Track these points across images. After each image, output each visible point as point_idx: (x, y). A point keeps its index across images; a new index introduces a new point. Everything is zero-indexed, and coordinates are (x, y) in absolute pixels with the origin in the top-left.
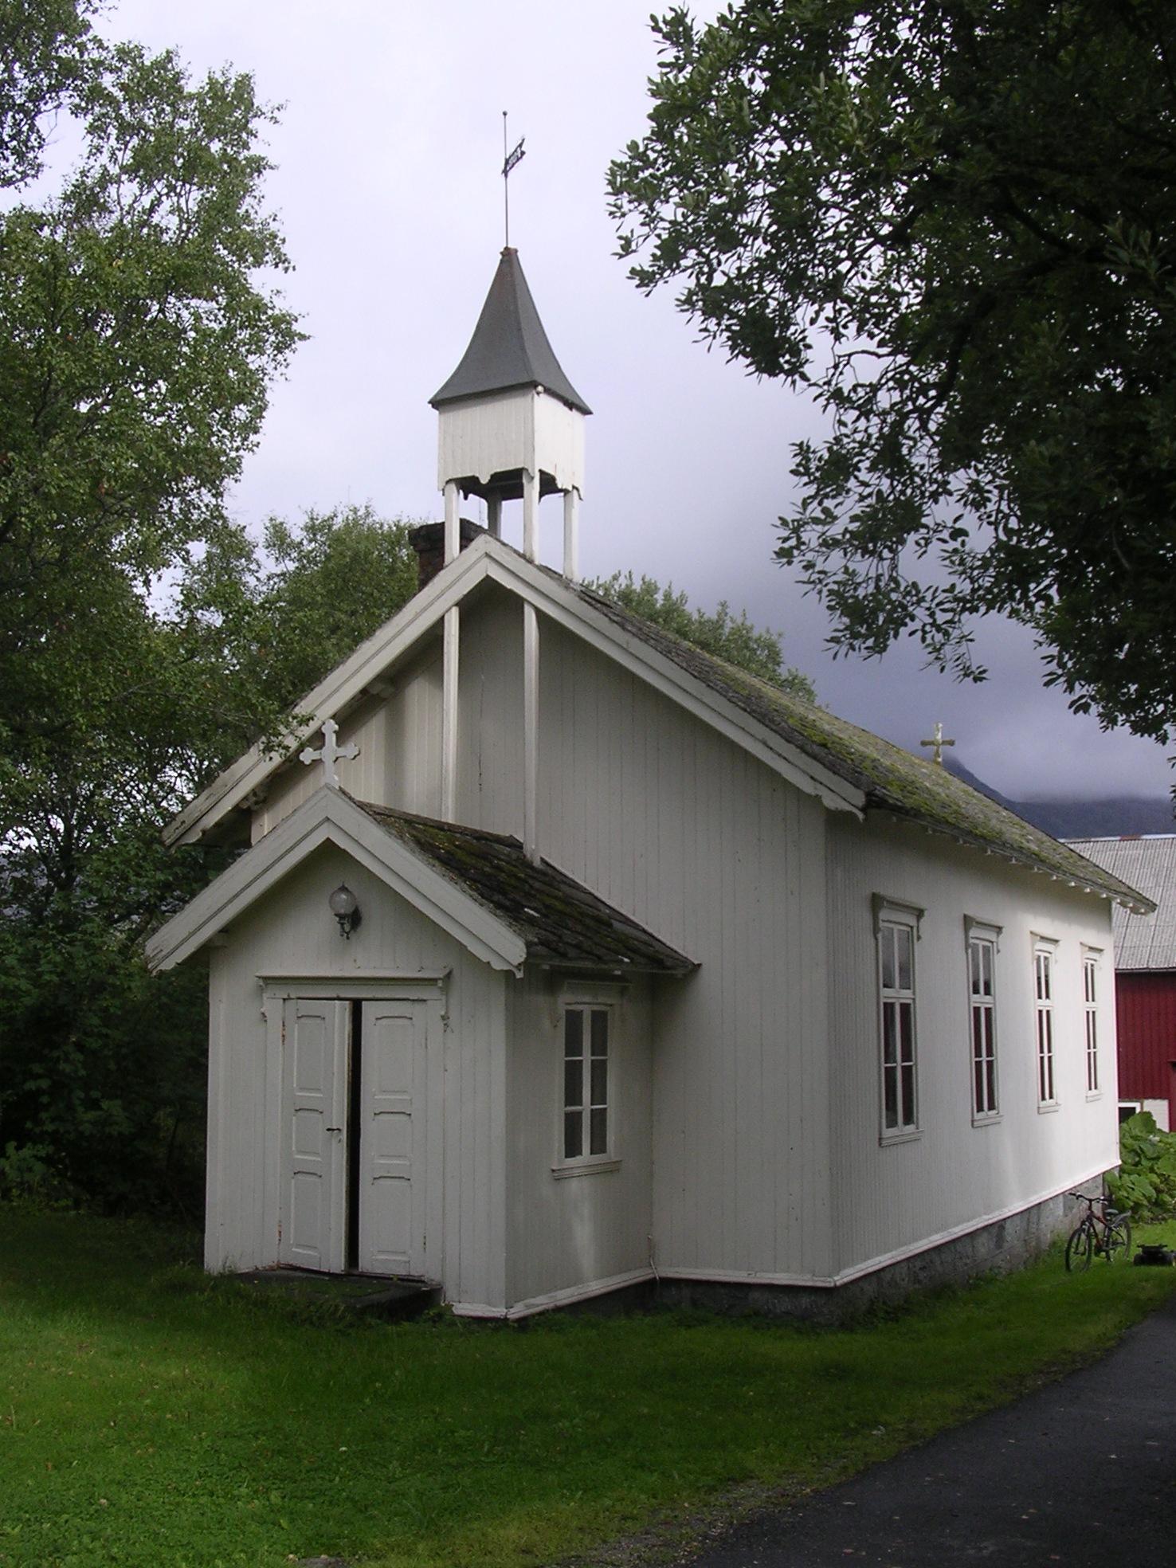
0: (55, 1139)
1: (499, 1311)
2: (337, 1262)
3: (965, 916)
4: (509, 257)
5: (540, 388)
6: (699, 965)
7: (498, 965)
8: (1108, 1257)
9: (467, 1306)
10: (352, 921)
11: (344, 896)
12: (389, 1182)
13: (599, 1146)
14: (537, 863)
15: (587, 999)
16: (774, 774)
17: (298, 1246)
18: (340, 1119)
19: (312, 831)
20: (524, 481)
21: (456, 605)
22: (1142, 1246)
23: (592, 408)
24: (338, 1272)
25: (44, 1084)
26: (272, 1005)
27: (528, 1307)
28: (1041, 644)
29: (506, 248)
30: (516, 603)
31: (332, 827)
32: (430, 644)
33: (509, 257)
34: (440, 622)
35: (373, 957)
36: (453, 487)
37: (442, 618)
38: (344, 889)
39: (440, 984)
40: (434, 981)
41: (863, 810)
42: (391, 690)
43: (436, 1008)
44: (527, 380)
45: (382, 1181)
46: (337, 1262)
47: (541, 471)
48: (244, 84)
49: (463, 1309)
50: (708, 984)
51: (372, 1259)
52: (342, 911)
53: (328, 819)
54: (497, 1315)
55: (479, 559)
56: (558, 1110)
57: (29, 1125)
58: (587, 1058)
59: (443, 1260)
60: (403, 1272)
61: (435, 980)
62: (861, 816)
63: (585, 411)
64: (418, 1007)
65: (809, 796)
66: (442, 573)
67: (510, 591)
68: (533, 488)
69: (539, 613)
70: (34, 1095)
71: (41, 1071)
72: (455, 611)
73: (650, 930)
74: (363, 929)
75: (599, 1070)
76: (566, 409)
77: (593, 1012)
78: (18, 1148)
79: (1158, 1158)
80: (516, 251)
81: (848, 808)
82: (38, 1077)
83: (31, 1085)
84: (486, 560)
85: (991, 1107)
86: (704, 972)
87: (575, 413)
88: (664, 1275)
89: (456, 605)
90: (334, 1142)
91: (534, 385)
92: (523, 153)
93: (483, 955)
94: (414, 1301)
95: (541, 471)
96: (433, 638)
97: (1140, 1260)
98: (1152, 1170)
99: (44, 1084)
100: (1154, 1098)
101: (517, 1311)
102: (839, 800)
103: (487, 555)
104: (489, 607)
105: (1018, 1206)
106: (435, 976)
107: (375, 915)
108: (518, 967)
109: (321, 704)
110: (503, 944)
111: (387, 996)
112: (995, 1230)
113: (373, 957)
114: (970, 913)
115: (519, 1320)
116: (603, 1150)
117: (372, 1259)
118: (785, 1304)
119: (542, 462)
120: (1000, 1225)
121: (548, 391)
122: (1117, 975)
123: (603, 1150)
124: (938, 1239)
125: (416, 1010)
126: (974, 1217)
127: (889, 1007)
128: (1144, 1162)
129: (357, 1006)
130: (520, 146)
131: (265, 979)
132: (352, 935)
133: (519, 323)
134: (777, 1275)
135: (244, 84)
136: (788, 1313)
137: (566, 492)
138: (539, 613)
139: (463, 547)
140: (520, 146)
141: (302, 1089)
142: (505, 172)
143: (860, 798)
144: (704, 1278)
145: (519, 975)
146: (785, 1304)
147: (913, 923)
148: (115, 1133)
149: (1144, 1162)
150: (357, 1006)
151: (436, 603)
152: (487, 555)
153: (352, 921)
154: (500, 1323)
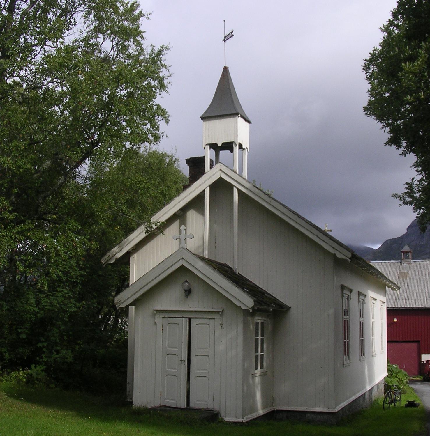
0: (46, 363)
1: (240, 420)
2: (183, 405)
3: (358, 292)
4: (226, 69)
5: (239, 115)
6: (290, 307)
7: (243, 307)
8: (395, 405)
9: (228, 418)
10: (188, 292)
11: (187, 284)
12: (200, 378)
13: (262, 367)
14: (237, 273)
15: (260, 318)
16: (320, 247)
17: (168, 399)
18: (184, 357)
19: (178, 261)
20: (234, 146)
21: (209, 186)
22: (408, 401)
23: (252, 122)
24: (184, 408)
25: (45, 344)
26: (159, 319)
27: (247, 418)
28: (401, 205)
29: (225, 67)
30: (231, 186)
31: (184, 261)
32: (199, 199)
33: (226, 69)
34: (204, 191)
35: (194, 305)
36: (208, 146)
37: (204, 191)
38: (186, 281)
39: (220, 313)
40: (218, 312)
41: (350, 259)
42: (182, 213)
43: (218, 321)
44: (235, 112)
45: (198, 378)
46: (183, 405)
47: (239, 143)
48: (364, 107)
49: (227, 419)
50: (293, 312)
51: (192, 405)
52: (186, 289)
53: (182, 258)
54: (240, 421)
55: (217, 171)
56: (253, 354)
57: (38, 359)
58: (259, 338)
59: (220, 403)
60: (205, 407)
61: (219, 312)
62: (349, 260)
63: (249, 122)
64: (211, 320)
65: (332, 254)
66: (204, 175)
67: (229, 182)
68: (236, 149)
69: (239, 190)
70: (41, 348)
71: (44, 340)
72: (208, 188)
73: (274, 296)
74: (192, 294)
75: (262, 340)
76: (245, 122)
77: (261, 322)
78: (35, 367)
79: (398, 373)
80: (228, 68)
81: (345, 258)
82: (42, 342)
83: (40, 345)
84: (220, 172)
85: (363, 355)
86: (292, 309)
87: (247, 123)
88: (277, 409)
89: (209, 186)
90: (182, 365)
91: (238, 114)
92: (232, 35)
93: (239, 304)
94: (212, 417)
95: (239, 143)
96: (200, 197)
97: (407, 406)
98: (396, 377)
99: (45, 344)
100: (425, 353)
101: (245, 420)
102: (342, 255)
103: (221, 170)
104: (221, 187)
105: (368, 388)
106: (219, 311)
107: (197, 290)
108: (251, 308)
109: (160, 217)
110: (247, 301)
111: (173, 316)
112: (361, 398)
113: (194, 305)
114: (359, 291)
115: (247, 422)
116: (263, 368)
117: (192, 405)
118: (319, 418)
119: (239, 140)
120: (364, 394)
121: (242, 117)
122: (387, 309)
123: (263, 368)
124: (354, 398)
125: (211, 322)
126: (359, 392)
127: (345, 321)
128: (394, 374)
129: (190, 319)
130: (232, 33)
131: (157, 311)
132: (188, 297)
133: (231, 93)
134: (316, 409)
135: (364, 107)
136: (320, 421)
137: (244, 149)
138: (239, 190)
139: (211, 168)
140: (232, 33)
141: (170, 347)
142: (225, 41)
143: (350, 255)
144: (297, 410)
145: (251, 311)
146: (319, 418)
147: (349, 294)
148: (69, 362)
149: (394, 374)
150: (190, 319)
151: (203, 185)
152: (221, 170)
153: (188, 292)
154: (241, 424)
